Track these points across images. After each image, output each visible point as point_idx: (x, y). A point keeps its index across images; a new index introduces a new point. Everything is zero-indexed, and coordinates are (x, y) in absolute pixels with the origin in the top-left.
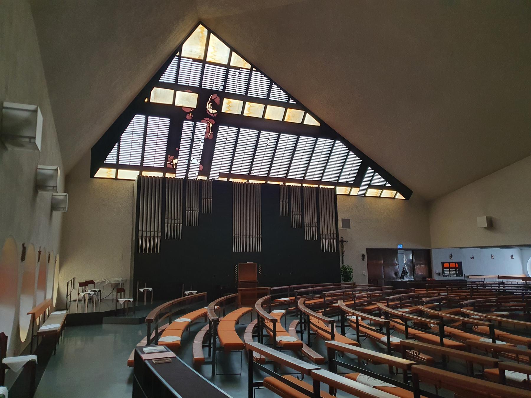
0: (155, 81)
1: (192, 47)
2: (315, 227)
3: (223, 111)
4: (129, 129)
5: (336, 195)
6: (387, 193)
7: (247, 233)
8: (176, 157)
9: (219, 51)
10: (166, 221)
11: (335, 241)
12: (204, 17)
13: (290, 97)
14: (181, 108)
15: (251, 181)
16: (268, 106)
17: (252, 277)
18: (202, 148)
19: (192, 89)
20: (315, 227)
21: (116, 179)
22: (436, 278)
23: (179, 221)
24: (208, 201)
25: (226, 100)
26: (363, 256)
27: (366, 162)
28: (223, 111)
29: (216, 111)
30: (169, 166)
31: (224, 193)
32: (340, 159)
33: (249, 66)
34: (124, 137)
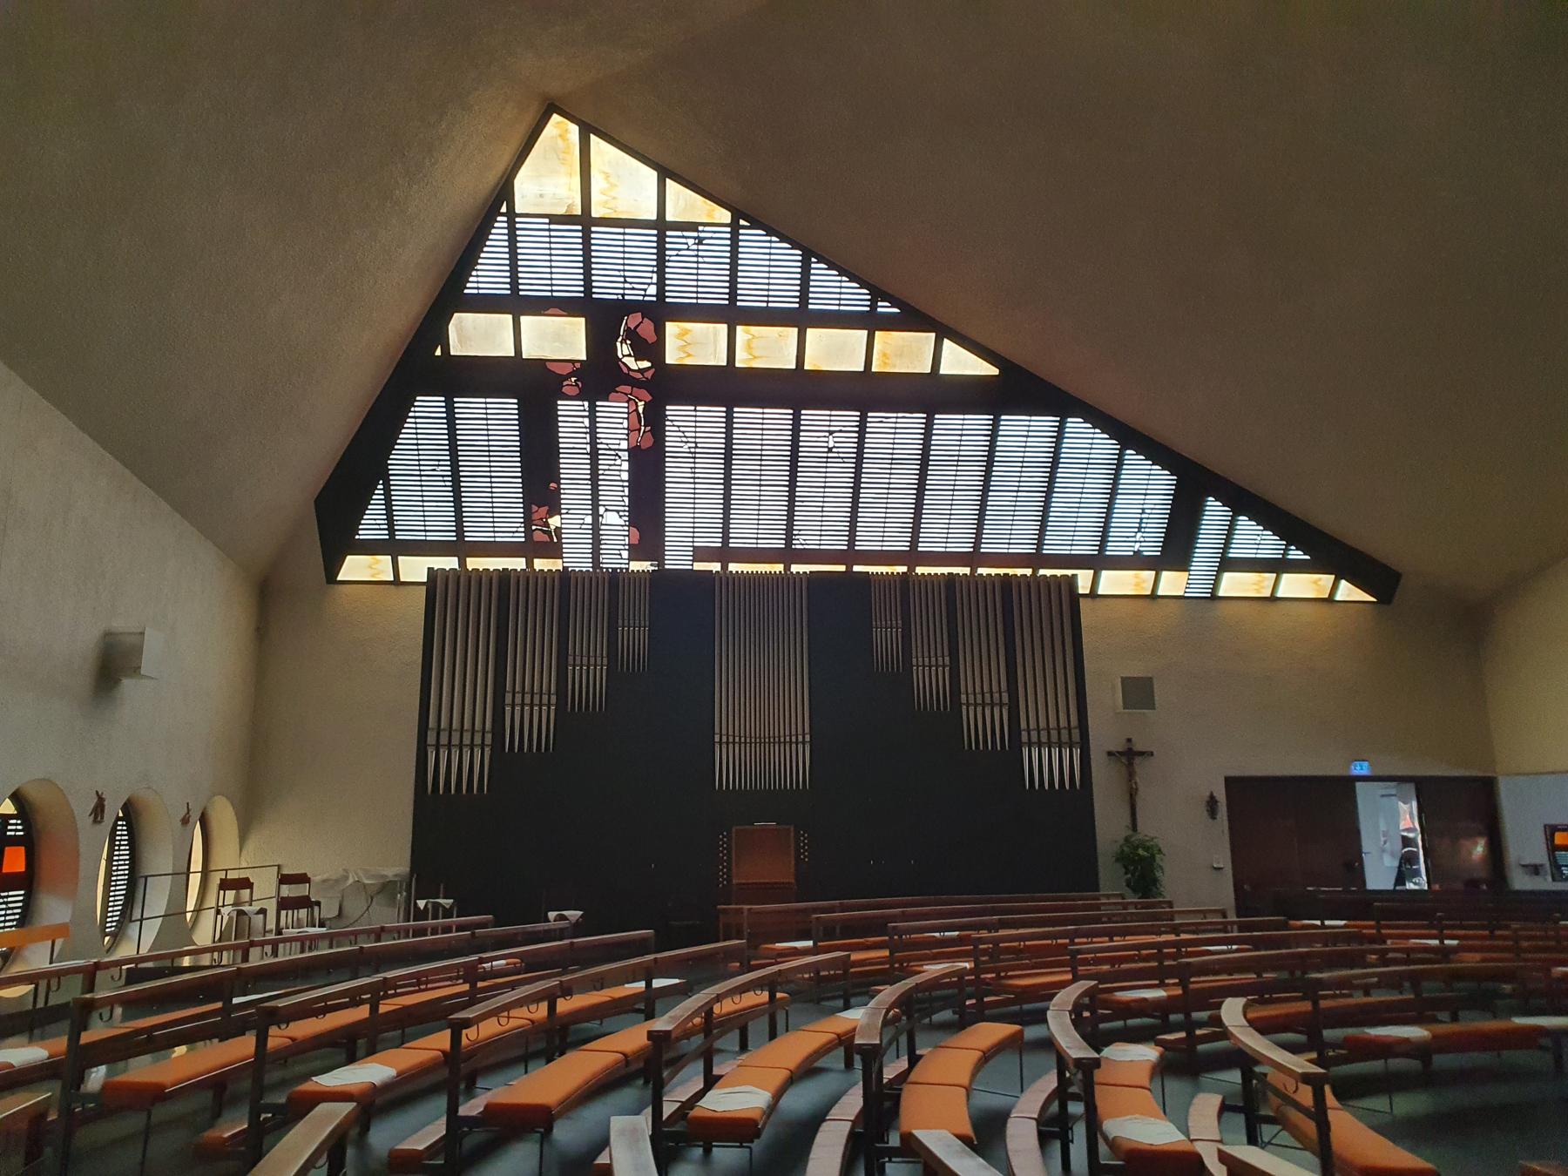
0: (452, 295)
1: (545, 183)
2: (1001, 705)
3: (670, 359)
4: (406, 436)
5: (1075, 598)
6: (1295, 585)
7: (762, 726)
8: (555, 509)
9: (626, 184)
10: (508, 699)
11: (1077, 752)
12: (555, 88)
13: (877, 294)
14: (541, 363)
15: (734, 567)
16: (809, 331)
17: (781, 870)
18: (625, 476)
19: (567, 306)
20: (1001, 705)
21: (397, 582)
22: (1521, 882)
23: (545, 698)
24: (635, 636)
25: (671, 328)
26: (1212, 803)
27: (1193, 487)
28: (670, 359)
29: (648, 364)
30: (539, 537)
31: (684, 612)
32: (1098, 481)
33: (725, 216)
34: (400, 461)
